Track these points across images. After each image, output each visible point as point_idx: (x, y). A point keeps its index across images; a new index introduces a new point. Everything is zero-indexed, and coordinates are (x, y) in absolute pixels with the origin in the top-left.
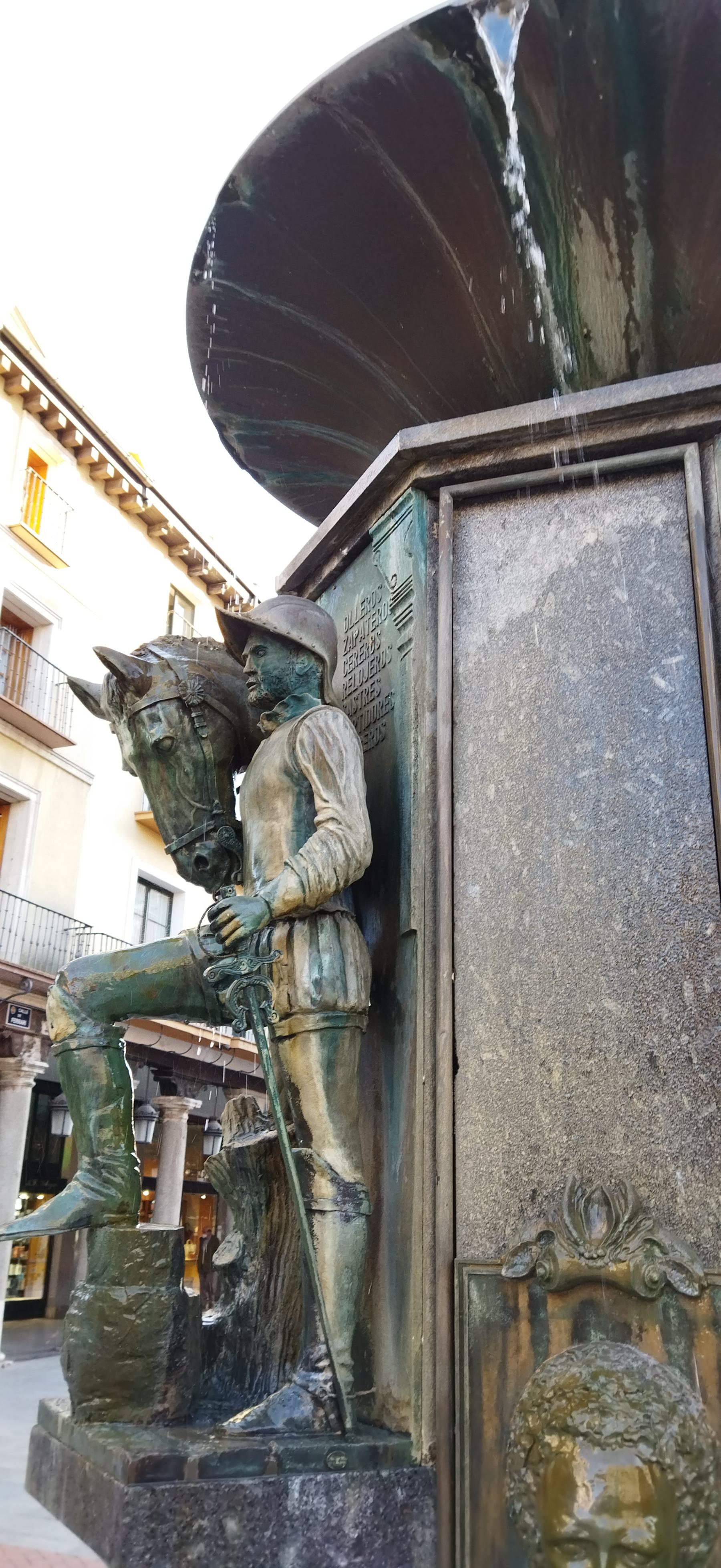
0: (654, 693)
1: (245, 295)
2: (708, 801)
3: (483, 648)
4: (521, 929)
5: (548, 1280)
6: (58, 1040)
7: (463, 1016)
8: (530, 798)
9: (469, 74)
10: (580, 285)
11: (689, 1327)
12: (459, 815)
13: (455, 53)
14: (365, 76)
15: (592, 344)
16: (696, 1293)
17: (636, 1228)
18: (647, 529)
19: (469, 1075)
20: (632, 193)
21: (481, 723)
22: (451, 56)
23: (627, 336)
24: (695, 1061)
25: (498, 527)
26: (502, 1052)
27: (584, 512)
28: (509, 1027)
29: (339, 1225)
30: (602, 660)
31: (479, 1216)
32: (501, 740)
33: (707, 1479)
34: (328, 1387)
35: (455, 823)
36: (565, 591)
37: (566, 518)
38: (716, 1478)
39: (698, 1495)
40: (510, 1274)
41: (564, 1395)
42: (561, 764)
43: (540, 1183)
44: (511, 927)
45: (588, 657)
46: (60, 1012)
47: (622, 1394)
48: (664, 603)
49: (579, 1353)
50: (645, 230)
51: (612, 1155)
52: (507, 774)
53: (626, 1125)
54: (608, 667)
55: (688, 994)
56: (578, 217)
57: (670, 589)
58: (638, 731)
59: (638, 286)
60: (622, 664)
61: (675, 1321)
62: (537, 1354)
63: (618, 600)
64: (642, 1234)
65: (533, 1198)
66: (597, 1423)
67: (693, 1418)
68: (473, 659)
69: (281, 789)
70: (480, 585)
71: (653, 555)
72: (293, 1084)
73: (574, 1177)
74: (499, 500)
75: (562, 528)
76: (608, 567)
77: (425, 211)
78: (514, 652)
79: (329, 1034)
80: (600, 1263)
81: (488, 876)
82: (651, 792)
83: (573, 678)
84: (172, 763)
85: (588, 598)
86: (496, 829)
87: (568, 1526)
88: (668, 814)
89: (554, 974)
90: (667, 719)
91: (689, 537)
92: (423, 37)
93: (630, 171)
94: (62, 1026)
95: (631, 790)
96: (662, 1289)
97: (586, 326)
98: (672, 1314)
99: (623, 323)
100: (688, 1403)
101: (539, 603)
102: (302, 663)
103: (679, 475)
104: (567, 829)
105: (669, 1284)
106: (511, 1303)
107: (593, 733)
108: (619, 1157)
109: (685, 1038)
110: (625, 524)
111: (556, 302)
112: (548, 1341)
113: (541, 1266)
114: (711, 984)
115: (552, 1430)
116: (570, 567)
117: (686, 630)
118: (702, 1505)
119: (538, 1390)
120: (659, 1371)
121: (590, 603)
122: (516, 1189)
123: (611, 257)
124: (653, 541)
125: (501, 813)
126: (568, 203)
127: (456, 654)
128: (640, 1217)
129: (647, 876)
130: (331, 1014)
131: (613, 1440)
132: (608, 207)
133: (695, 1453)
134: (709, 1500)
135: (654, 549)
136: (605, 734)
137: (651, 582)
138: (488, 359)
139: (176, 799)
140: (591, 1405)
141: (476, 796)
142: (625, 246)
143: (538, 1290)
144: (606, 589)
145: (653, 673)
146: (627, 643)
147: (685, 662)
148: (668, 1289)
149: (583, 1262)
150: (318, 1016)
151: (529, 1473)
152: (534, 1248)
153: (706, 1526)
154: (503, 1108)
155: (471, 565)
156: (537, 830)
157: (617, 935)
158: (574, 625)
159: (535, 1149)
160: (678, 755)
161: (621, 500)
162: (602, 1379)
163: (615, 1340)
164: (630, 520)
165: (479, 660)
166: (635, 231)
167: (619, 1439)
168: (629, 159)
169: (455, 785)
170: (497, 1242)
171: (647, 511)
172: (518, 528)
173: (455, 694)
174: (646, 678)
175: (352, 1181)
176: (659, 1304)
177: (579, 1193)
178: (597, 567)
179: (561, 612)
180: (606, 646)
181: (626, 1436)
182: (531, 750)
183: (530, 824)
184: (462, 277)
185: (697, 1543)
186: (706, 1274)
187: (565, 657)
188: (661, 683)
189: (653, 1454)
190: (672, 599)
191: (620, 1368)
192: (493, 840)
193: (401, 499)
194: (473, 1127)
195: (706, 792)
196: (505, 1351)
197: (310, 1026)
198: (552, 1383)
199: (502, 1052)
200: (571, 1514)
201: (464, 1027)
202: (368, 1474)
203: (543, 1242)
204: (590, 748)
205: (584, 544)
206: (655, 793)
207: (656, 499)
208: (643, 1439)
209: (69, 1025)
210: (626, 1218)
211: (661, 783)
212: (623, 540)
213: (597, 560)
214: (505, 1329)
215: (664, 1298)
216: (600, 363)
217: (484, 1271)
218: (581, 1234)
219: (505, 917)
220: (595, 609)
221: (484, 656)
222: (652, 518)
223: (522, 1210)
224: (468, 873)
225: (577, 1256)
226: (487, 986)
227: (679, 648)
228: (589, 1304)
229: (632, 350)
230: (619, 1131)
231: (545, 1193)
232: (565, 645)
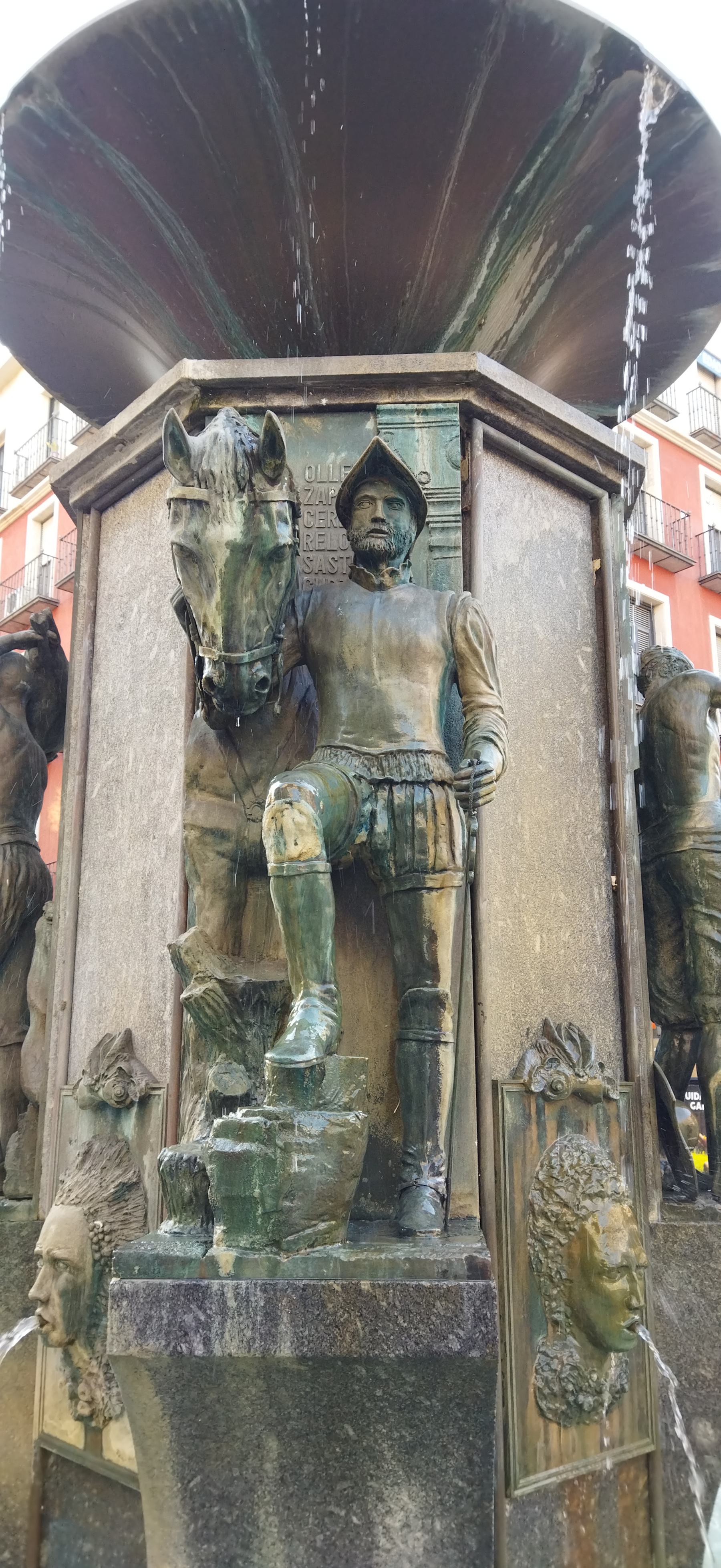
1: (246, 38)
6: (302, 859)
9: (589, 91)
10: (503, 286)
13: (600, 71)
14: (547, 20)
20: (569, 251)
22: (596, 70)
46: (310, 830)
56: (536, 239)
65: (527, 1034)
69: (435, 658)
72: (433, 931)
77: (464, 137)
84: (272, 569)
92: (604, 43)
93: (579, 238)
94: (309, 845)
99: (502, 335)
111: (484, 285)
112: (546, 1136)
123: (528, 283)
126: (540, 224)
132: (554, 247)
138: (412, 285)
139: (258, 609)
142: (540, 282)
184: (442, 208)
193: (440, 406)
196: (525, 1147)
209: (316, 845)
214: (524, 1130)
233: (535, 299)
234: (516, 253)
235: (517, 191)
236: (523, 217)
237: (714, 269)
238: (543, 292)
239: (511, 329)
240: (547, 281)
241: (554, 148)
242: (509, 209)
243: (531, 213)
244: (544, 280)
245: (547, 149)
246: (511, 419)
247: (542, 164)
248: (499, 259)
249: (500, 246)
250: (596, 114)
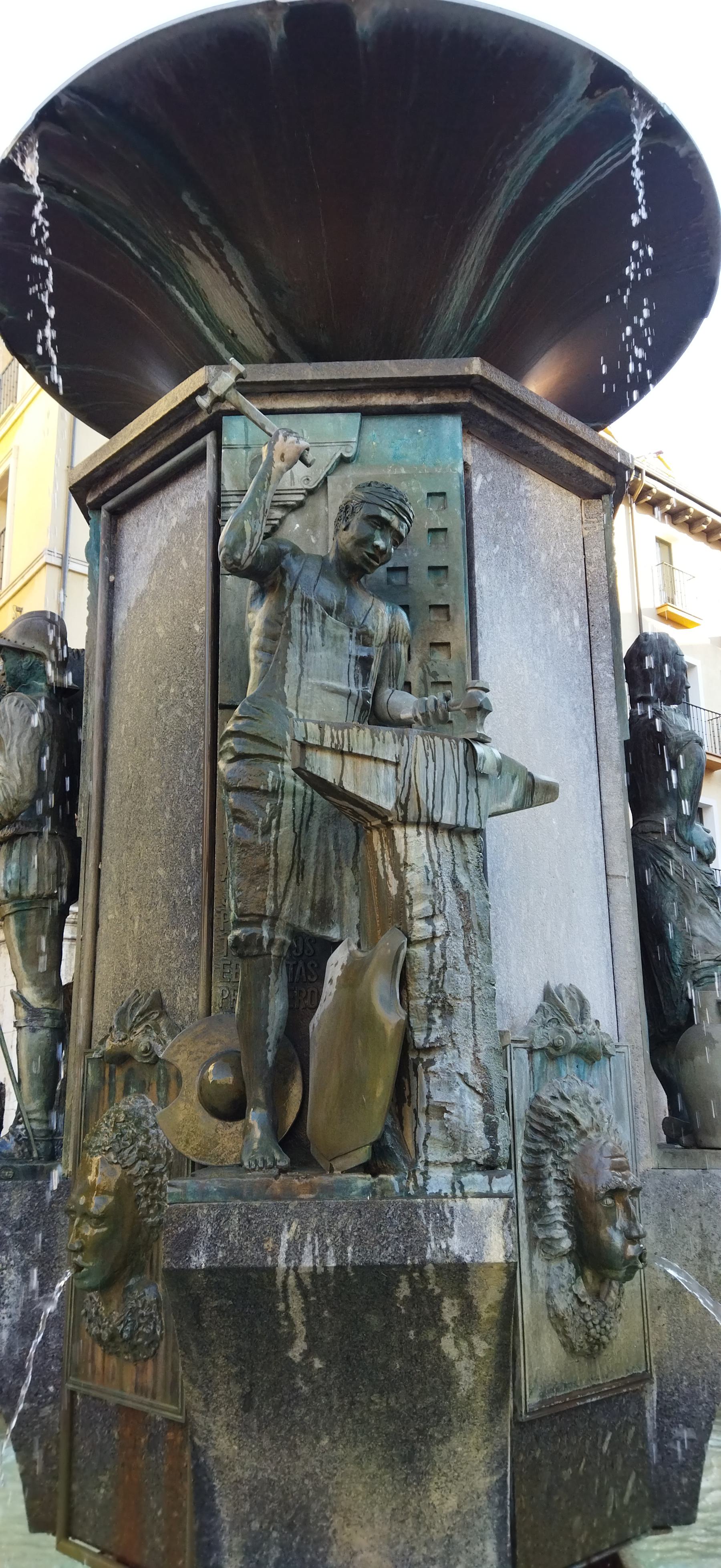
10: (209, 300)
15: (239, 338)
23: (258, 324)
29: (29, 1034)
34: (23, 1132)
50: (228, 242)
56: (182, 252)
59: (246, 287)
79: (20, 914)
93: (193, 207)
97: (229, 328)
99: (250, 317)
102: (26, 662)
111: (202, 318)
123: (217, 271)
130: (17, 902)
132: (194, 235)
150: (10, 905)
166: (223, 247)
168: (186, 197)
175: (40, 1007)
185: (153, 1216)
197: (7, 911)
202: (28, 1182)
216: (253, 352)
229: (268, 333)
233: (235, 268)
234: (188, 274)
235: (139, 257)
236: (161, 257)
237: (282, 32)
238: (234, 258)
239: (250, 305)
240: (225, 250)
241: (106, 219)
242: (153, 269)
243: (158, 249)
244: (222, 253)
245: (106, 225)
246: (115, 480)
247: (118, 231)
248: (188, 292)
249: (178, 288)
250: (72, 183)
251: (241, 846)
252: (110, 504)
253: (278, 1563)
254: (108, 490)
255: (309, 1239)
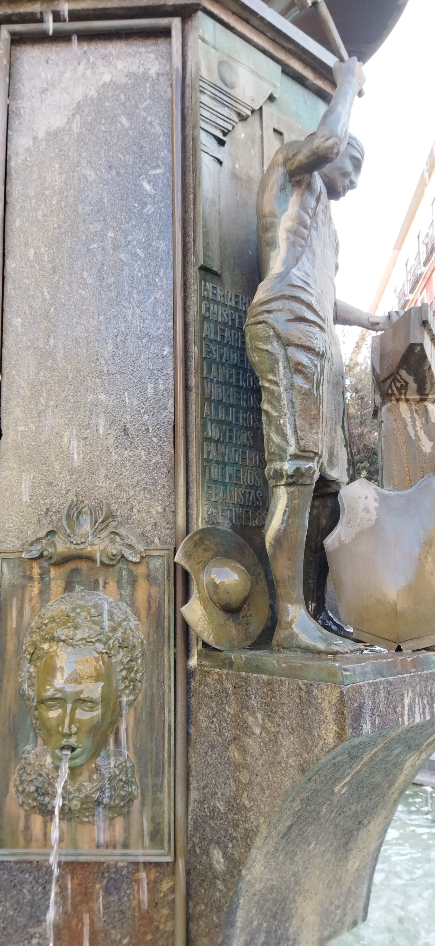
0: (143, 194)
2: (171, 270)
3: (28, 150)
4: (48, 347)
5: (50, 558)
7: (6, 403)
8: (58, 260)
11: (133, 581)
12: (8, 268)
16: (138, 560)
17: (107, 526)
18: (145, 77)
19: (9, 440)
21: (26, 204)
24: (150, 431)
25: (44, 62)
26: (31, 426)
27: (103, 59)
28: (37, 410)
30: (110, 167)
31: (12, 525)
32: (39, 217)
33: (136, 661)
35: (5, 274)
36: (88, 115)
37: (91, 61)
38: (142, 660)
39: (130, 670)
40: (28, 556)
41: (54, 621)
42: (79, 238)
43: (51, 504)
44: (41, 346)
45: (101, 164)
47: (88, 617)
48: (153, 130)
49: (67, 598)
51: (97, 486)
52: (42, 242)
53: (107, 469)
54: (114, 172)
55: (150, 391)
57: (157, 121)
58: (130, 219)
60: (122, 171)
61: (125, 577)
62: (42, 600)
63: (123, 125)
64: (110, 529)
65: (46, 513)
66: (71, 633)
67: (131, 629)
68: (21, 158)
70: (29, 103)
71: (148, 95)
73: (72, 500)
74: (45, 42)
75: (87, 69)
76: (117, 101)
78: (51, 155)
80: (82, 546)
81: (27, 312)
82: (136, 261)
83: (90, 178)
85: (103, 121)
86: (33, 280)
87: (50, 692)
88: (146, 276)
89: (68, 377)
90: (149, 213)
91: (171, 85)
95: (123, 259)
96: (119, 559)
98: (124, 573)
100: (130, 621)
101: (70, 121)
103: (168, 40)
104: (81, 283)
105: (123, 557)
106: (28, 573)
107: (101, 218)
108: (100, 487)
109: (146, 417)
110: (131, 71)
113: (46, 550)
114: (164, 384)
115: (45, 640)
116: (91, 97)
117: (166, 152)
118: (132, 675)
119: (40, 620)
120: (114, 604)
121: (104, 125)
122: (36, 509)
124: (148, 85)
125: (38, 269)
127: (9, 152)
128: (110, 520)
129: (130, 316)
131: (81, 642)
133: (130, 647)
134: (137, 672)
135: (148, 91)
136: (109, 220)
137: (145, 114)
140: (69, 624)
141: (21, 256)
143: (46, 564)
144: (115, 116)
145: (143, 179)
146: (127, 157)
147: (164, 174)
148: (123, 559)
149: (72, 546)
151: (32, 666)
152: (44, 541)
153: (134, 686)
154: (30, 460)
155: (22, 88)
156: (61, 282)
157: (109, 353)
158: (93, 140)
159: (50, 484)
160: (155, 238)
161: (129, 54)
162: (78, 610)
163: (89, 590)
164: (134, 68)
165: (26, 158)
167: (84, 642)
169: (6, 247)
170: (22, 540)
171: (145, 63)
172: (57, 65)
173: (8, 181)
174: (138, 183)
176: (117, 568)
177: (75, 509)
178: (110, 100)
179: (84, 129)
180: (113, 157)
181: (89, 640)
182: (59, 227)
183: (57, 278)
186: (145, 550)
187: (85, 162)
188: (147, 187)
189: (104, 649)
190: (158, 129)
191: (90, 604)
192: (31, 287)
194: (10, 472)
195: (170, 263)
198: (49, 615)
199: (31, 426)
200: (52, 685)
201: (6, 410)
203: (49, 537)
204: (99, 229)
205: (102, 82)
206: (139, 262)
207: (152, 56)
208: (98, 640)
210: (100, 520)
211: (143, 256)
212: (129, 82)
213: (110, 94)
215: (120, 565)
217: (12, 556)
218: (73, 531)
219: (38, 340)
220: (107, 130)
221: (30, 156)
222: (149, 69)
223: (39, 521)
224: (14, 309)
225: (69, 543)
226: (23, 384)
227: (160, 163)
228: (76, 571)
230: (102, 472)
231: (54, 510)
232: (85, 154)
251: (303, 394)
252: (18, 28)
253: (264, 943)
254: (20, 14)
255: (417, 702)
